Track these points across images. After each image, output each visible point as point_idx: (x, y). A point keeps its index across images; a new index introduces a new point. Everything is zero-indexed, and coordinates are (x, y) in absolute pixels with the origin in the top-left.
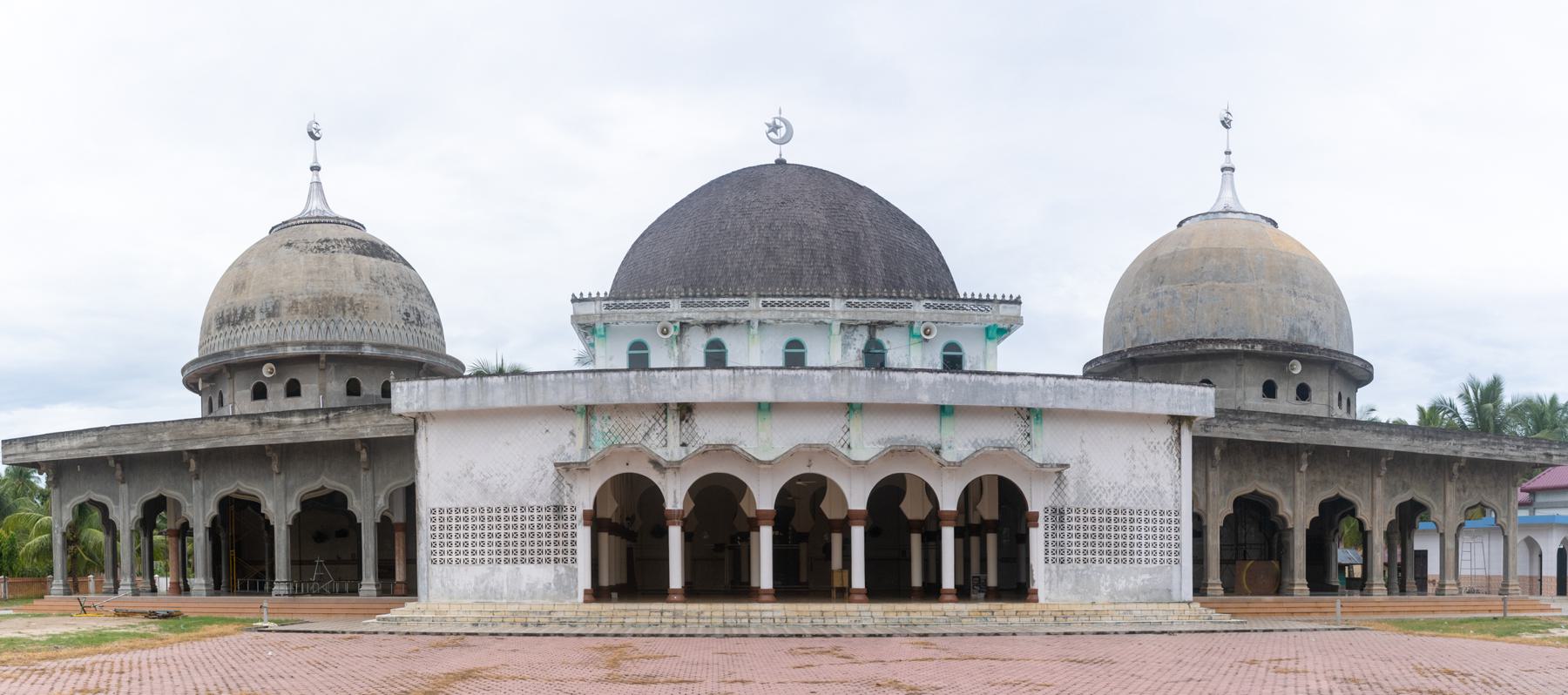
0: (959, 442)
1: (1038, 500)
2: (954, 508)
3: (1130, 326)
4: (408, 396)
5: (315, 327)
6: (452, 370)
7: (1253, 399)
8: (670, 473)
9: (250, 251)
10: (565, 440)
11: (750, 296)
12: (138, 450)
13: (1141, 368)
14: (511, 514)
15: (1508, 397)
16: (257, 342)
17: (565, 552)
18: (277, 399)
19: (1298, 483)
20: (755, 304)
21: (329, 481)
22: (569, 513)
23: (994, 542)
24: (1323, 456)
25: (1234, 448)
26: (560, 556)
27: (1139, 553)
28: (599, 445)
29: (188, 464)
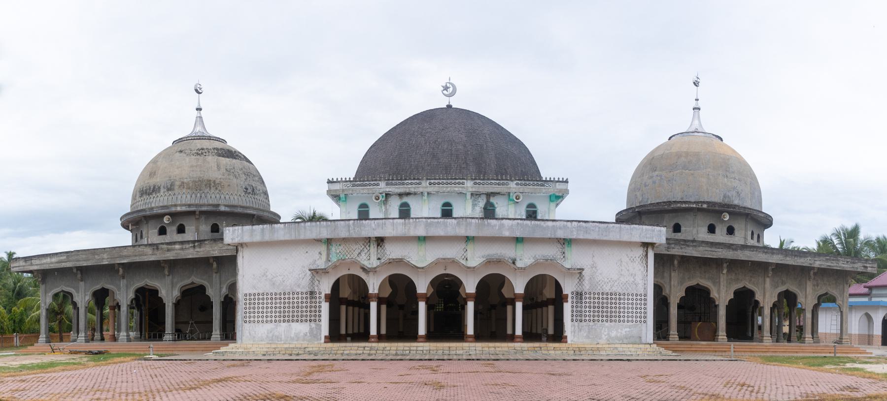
0: (526, 257)
1: (568, 289)
2: (522, 292)
3: (638, 194)
4: (232, 234)
5: (194, 196)
6: (272, 219)
7: (703, 234)
8: (371, 274)
9: (160, 154)
10: (317, 257)
11: (422, 179)
12: (89, 263)
13: (643, 217)
14: (287, 296)
15: (862, 236)
16: (161, 204)
17: (315, 316)
18: (172, 235)
19: (722, 280)
20: (425, 183)
21: (197, 279)
22: (318, 296)
23: (543, 310)
24: (734, 265)
25: (685, 261)
26: (313, 318)
27: (624, 317)
28: (334, 259)
29: (118, 271)
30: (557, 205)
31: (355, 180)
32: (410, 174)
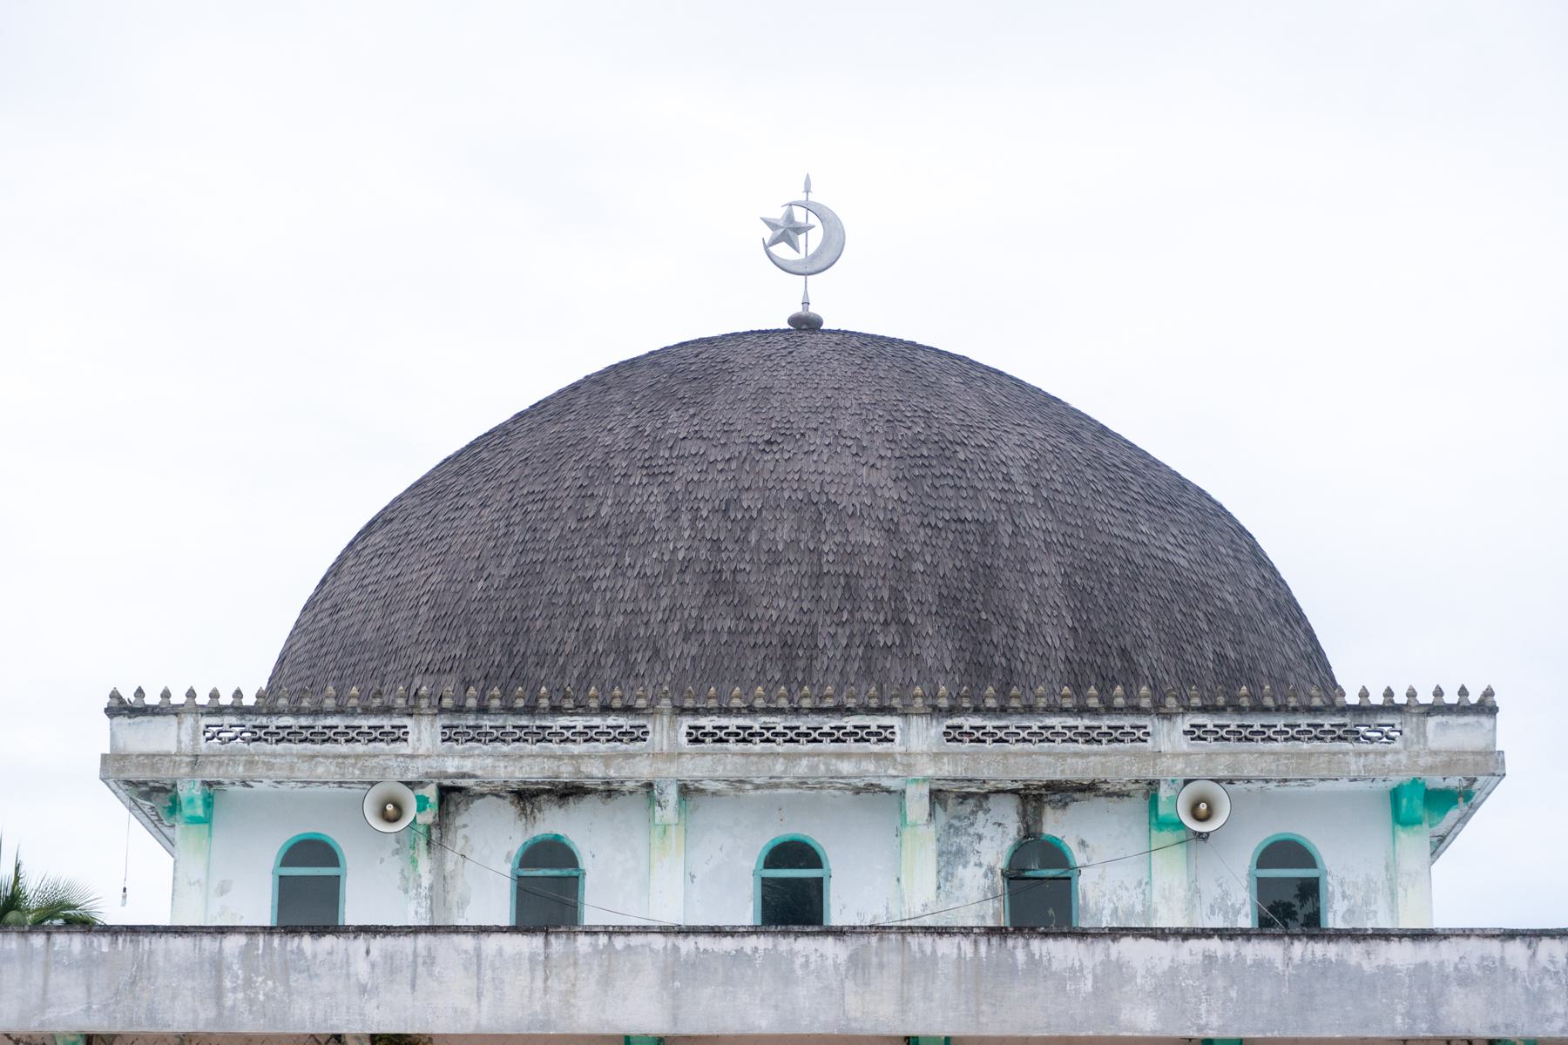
11: (651, 711)
20: (668, 733)
30: (1439, 843)
31: (267, 704)
32: (584, 681)
